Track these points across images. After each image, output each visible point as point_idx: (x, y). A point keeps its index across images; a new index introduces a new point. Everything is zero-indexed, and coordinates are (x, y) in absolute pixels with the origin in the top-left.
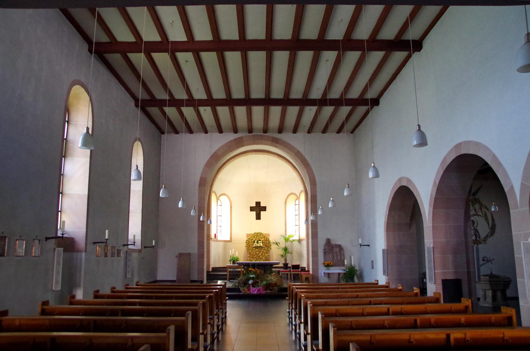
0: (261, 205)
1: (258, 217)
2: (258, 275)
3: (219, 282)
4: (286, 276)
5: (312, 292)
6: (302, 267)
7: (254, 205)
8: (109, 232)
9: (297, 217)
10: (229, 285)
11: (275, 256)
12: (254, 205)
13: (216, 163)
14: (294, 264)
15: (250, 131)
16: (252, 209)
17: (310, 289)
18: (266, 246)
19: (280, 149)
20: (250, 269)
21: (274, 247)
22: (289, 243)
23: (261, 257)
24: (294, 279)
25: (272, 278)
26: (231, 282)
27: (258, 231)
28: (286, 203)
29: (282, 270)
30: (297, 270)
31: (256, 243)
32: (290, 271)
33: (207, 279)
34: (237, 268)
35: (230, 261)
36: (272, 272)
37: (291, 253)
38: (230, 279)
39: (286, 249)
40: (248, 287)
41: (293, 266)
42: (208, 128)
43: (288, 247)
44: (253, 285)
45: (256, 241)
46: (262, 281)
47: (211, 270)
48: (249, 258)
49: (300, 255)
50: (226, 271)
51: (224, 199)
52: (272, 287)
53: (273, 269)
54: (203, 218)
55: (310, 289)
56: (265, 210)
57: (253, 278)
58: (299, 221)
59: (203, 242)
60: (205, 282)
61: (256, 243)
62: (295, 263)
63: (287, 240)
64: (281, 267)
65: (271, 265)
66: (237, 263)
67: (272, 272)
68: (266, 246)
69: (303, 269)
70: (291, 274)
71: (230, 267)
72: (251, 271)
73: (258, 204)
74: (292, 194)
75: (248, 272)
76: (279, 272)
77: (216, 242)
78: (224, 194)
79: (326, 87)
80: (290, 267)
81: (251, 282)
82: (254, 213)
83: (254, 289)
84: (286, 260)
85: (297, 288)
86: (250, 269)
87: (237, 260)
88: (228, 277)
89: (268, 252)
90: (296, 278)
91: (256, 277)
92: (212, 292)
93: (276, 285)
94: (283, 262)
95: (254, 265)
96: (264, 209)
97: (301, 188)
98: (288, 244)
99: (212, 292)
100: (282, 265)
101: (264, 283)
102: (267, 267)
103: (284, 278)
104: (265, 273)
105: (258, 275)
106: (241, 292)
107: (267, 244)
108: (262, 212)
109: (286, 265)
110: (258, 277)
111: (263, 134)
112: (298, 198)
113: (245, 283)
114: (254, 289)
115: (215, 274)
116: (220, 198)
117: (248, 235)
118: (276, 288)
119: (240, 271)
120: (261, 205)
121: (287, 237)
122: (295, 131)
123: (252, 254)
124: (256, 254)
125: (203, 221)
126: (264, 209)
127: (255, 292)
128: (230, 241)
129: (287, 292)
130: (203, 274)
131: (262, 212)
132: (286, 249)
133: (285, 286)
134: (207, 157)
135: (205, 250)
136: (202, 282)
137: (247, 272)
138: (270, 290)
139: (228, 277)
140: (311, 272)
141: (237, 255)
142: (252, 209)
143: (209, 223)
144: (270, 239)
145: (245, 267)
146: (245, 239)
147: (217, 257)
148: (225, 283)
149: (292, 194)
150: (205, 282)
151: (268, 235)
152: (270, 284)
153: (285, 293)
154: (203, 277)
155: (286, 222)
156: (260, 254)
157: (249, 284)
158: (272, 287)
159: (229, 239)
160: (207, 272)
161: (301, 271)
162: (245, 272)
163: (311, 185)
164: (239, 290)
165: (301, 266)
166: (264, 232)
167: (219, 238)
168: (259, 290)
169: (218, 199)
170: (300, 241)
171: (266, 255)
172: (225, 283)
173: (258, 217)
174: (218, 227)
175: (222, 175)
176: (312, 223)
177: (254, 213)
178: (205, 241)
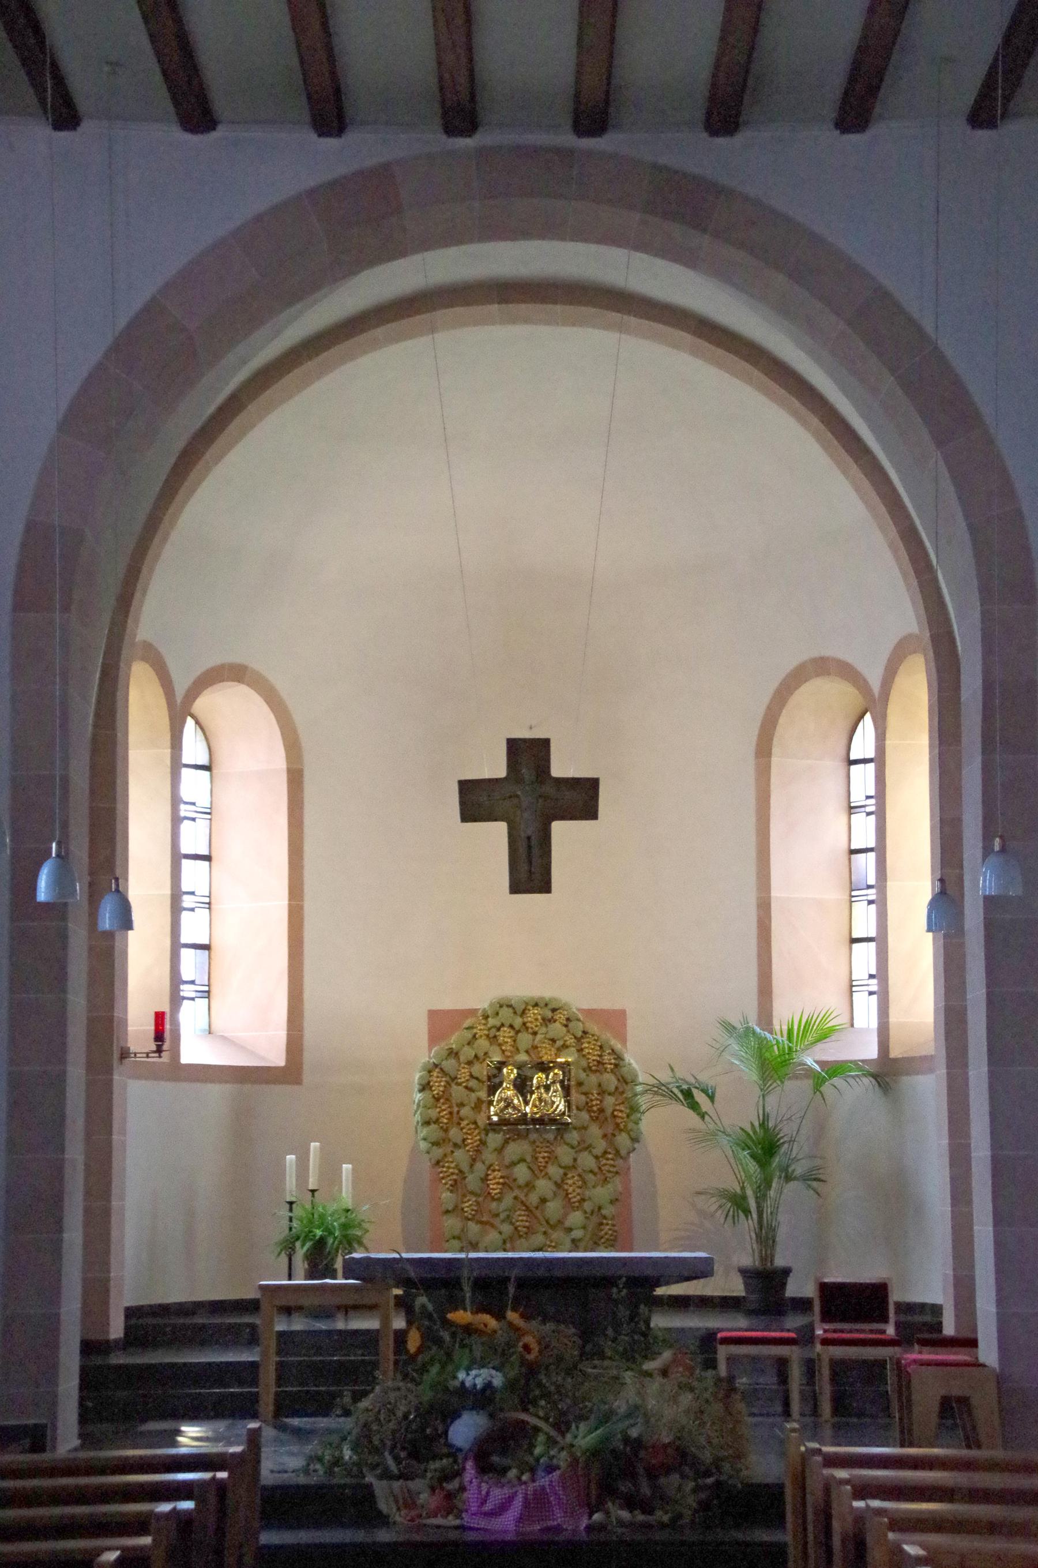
0: (557, 770)
1: (531, 872)
2: (531, 1370)
3: (191, 1437)
4: (769, 1380)
5: (992, 1528)
6: (907, 1308)
7: (494, 766)
8: (34, 888)
9: (867, 864)
10: (283, 1462)
11: (673, 1204)
12: (494, 766)
13: (162, 400)
14: (835, 1276)
15: (460, 112)
16: (476, 801)
17: (975, 1495)
18: (599, 1116)
19: (722, 273)
20: (461, 1316)
21: (660, 1124)
22: (795, 1090)
23: (553, 1208)
24: (839, 1405)
25: (651, 1399)
26: (299, 1433)
27: (522, 987)
28: (764, 750)
29: (736, 1324)
30: (864, 1330)
31: (508, 1091)
32: (805, 1337)
33: (84, 1419)
34: (347, 1309)
35: (288, 1247)
36: (644, 1344)
37: (813, 1178)
38: (285, 1406)
39: (765, 1146)
40: (446, 1476)
41: (825, 1289)
42: (83, 84)
43: (787, 1130)
44: (492, 1454)
45: (510, 1073)
46: (562, 1426)
47: (116, 1330)
48: (451, 1223)
49: (893, 1198)
50: (253, 1339)
51: (234, 713)
52: (652, 1474)
53: (660, 1321)
54: (62, 880)
55: (975, 1495)
56: (590, 812)
57: (483, 1399)
58: (881, 903)
59: (58, 1083)
60: (67, 1441)
61: (508, 1091)
62: (850, 1269)
63: (774, 1065)
64: (727, 1304)
65: (641, 1283)
66: (351, 1269)
67: (644, 1344)
68: (599, 1116)
69: (921, 1326)
70: (810, 1368)
71: (288, 1303)
72: (468, 1329)
73: (529, 754)
74: (822, 666)
75: (443, 1342)
76: (709, 1341)
77: (167, 1087)
78: (236, 673)
79: (993, 67)
80: (802, 1305)
81: (465, 1429)
82: (494, 836)
83: (498, 1494)
84: (766, 1238)
85: (863, 1491)
86: (461, 1316)
87: (350, 1242)
88: (268, 1389)
89: (613, 1161)
90: (860, 1398)
91: (511, 1385)
92: (141, 1525)
93: (681, 1457)
94: (747, 1259)
95: (493, 1286)
96: (582, 799)
97: (905, 617)
98: (788, 1099)
99: (141, 1525)
100: (736, 1287)
101: (584, 1437)
102: (602, 1303)
103: (751, 1396)
104: (590, 1351)
105: (531, 1370)
106: (383, 1520)
107: (606, 1095)
108: (559, 829)
109: (767, 1285)
110: (526, 1386)
111: (568, 139)
112: (875, 704)
113: (421, 1443)
114: (498, 1494)
115: (151, 1365)
116: (202, 704)
117: (441, 1023)
118: (683, 1491)
119: (369, 1340)
120: (557, 770)
121: (778, 1036)
122: (855, 111)
123: (472, 1181)
124: (508, 1183)
125: (57, 910)
126: (582, 799)
127: (506, 1525)
128: (290, 1073)
129: (780, 1521)
130: (51, 1371)
131: (559, 829)
132: (765, 1146)
133: (763, 1466)
134: (86, 352)
135: (75, 1152)
136: (38, 1438)
137: (430, 1338)
138: (630, 1503)
139: (268, 1389)
140: (988, 1353)
141: (346, 1195)
142: (476, 801)
143: (106, 921)
144: (630, 1058)
145: (422, 1300)
146: (422, 1054)
147: (169, 1225)
148: (254, 1440)
149: (822, 666)
150: (67, 1441)
151: (615, 1020)
152: (637, 1444)
153: (763, 1536)
154: (53, 1405)
155: (764, 907)
156: (543, 1186)
157: (454, 1452)
158: (652, 1474)
159: (276, 1057)
160: (88, 1348)
161: (901, 1341)
162: (414, 1342)
163: (985, 592)
164: (362, 1507)
165: (896, 1296)
166: (577, 996)
167: (195, 1049)
168: (537, 1503)
169: (179, 712)
170: (887, 1073)
171: (601, 1194)
172: (254, 1440)
173: (531, 872)
174: (187, 956)
175: (216, 506)
176: (989, 925)
177: (494, 836)
178: (76, 1074)
